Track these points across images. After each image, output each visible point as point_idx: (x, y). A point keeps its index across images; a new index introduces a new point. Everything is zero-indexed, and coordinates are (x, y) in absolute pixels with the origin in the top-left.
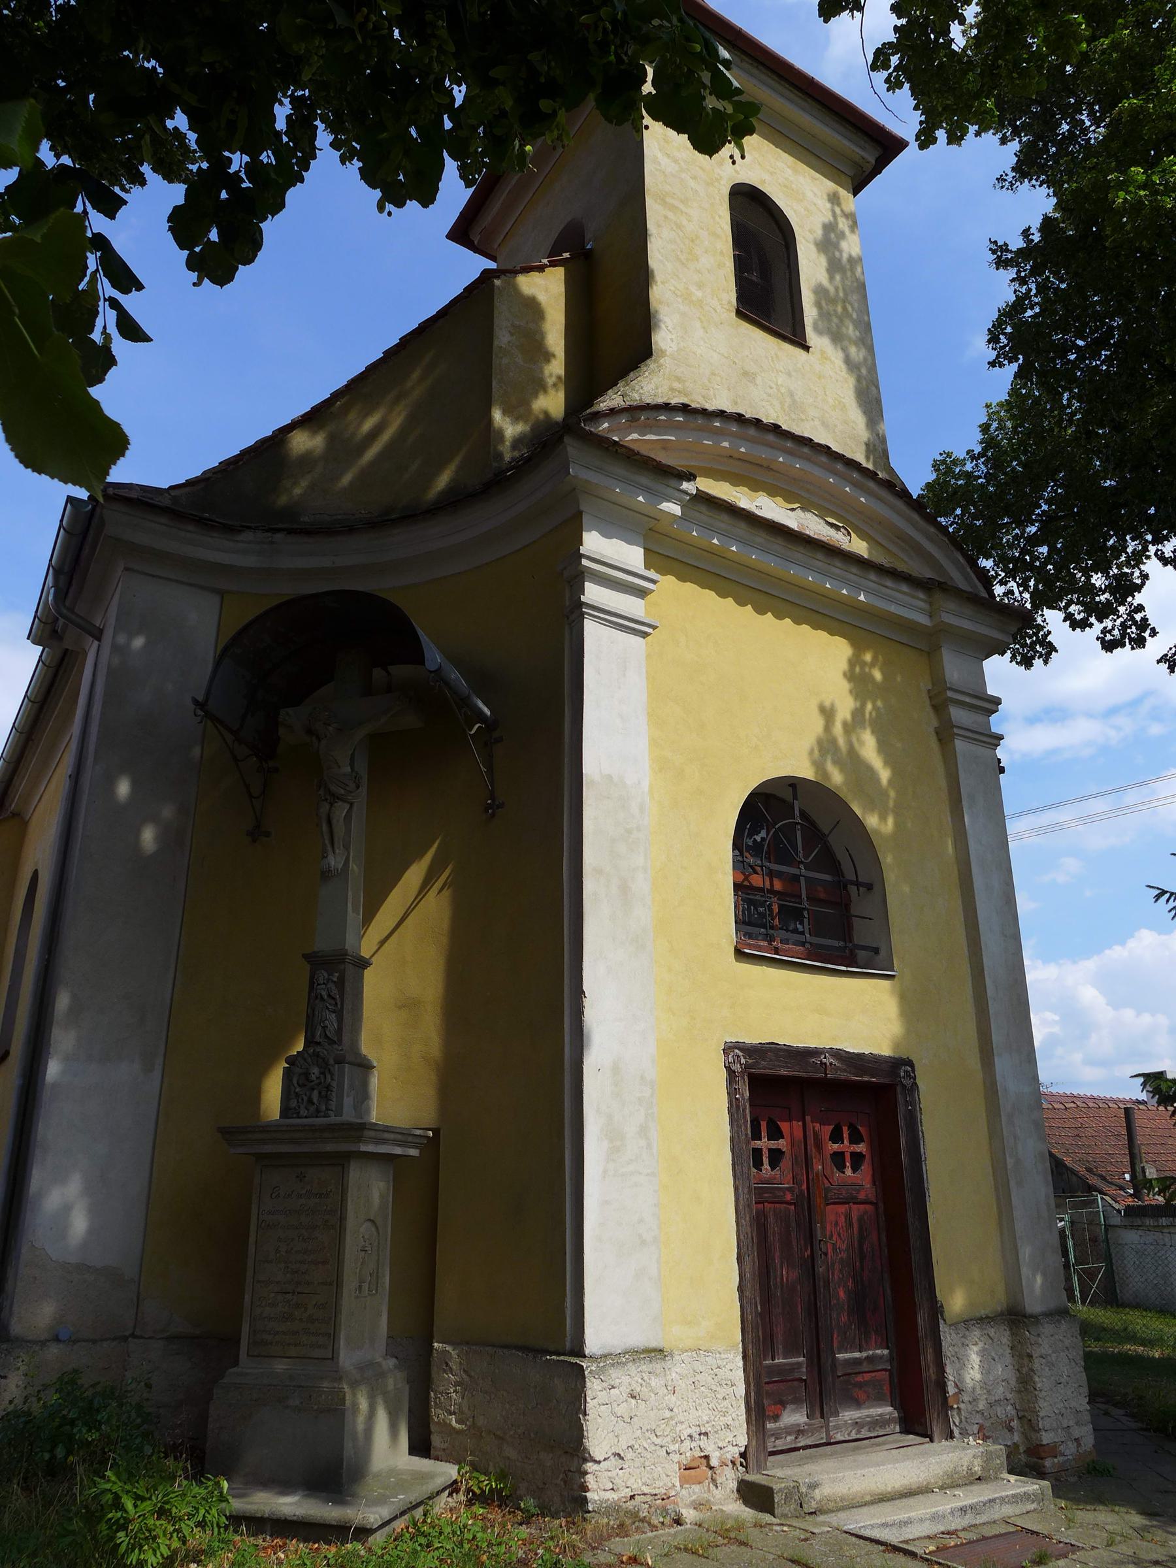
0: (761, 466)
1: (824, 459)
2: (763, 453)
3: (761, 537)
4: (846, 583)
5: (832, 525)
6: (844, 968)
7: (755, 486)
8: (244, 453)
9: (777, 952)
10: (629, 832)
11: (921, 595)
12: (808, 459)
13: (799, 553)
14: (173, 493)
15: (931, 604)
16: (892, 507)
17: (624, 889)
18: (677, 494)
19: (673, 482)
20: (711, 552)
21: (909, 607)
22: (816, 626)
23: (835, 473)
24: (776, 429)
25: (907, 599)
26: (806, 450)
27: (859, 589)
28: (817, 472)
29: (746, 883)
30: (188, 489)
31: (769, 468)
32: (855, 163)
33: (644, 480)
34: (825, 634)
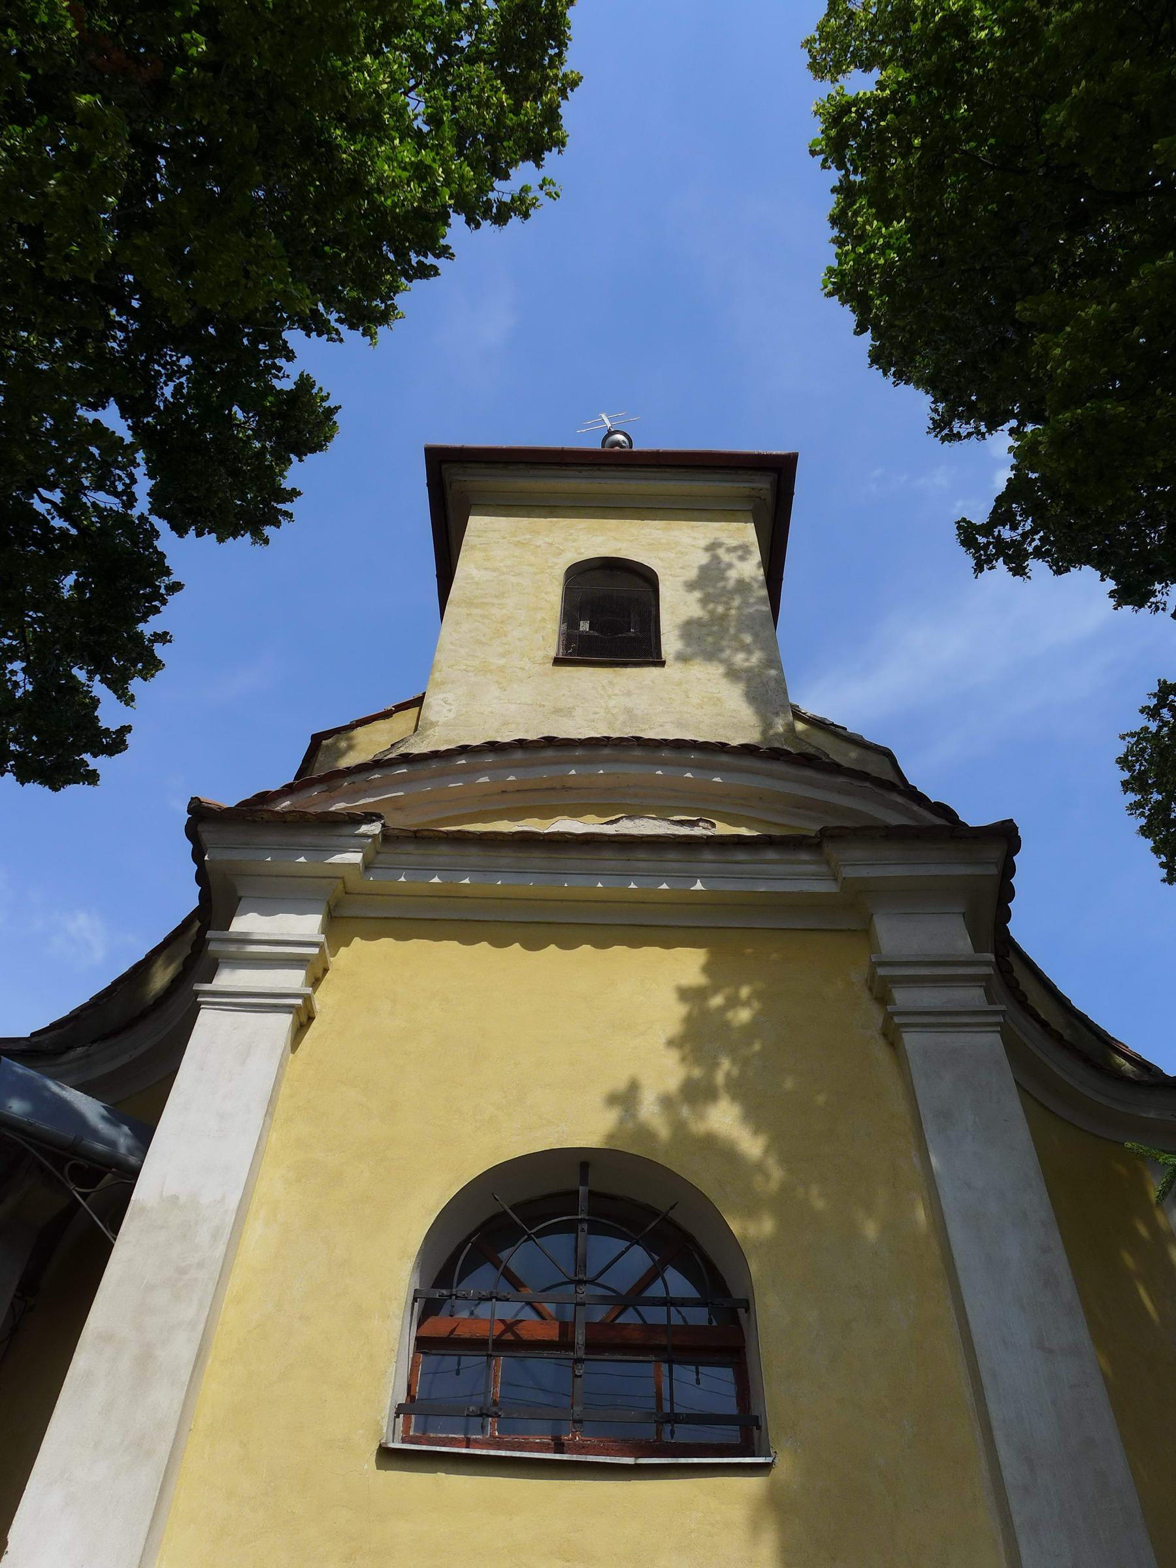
0: (554, 789)
1: (638, 753)
2: (544, 774)
3: (506, 858)
4: (664, 875)
5: (681, 823)
6: (630, 1461)
7: (549, 812)
8: (116, 983)
9: (559, 1447)
10: (182, 1271)
11: (804, 856)
12: (616, 761)
13: (573, 859)
14: (35, 1040)
15: (828, 863)
16: (769, 775)
17: (145, 1359)
18: (353, 841)
19: (347, 830)
20: (437, 895)
21: (802, 878)
22: (635, 943)
23: (663, 763)
24: (550, 742)
25: (780, 868)
26: (606, 751)
27: (693, 878)
28: (634, 770)
29: (509, 1336)
30: (55, 1033)
31: (565, 788)
32: (749, 497)
33: (307, 839)
34: (657, 950)
